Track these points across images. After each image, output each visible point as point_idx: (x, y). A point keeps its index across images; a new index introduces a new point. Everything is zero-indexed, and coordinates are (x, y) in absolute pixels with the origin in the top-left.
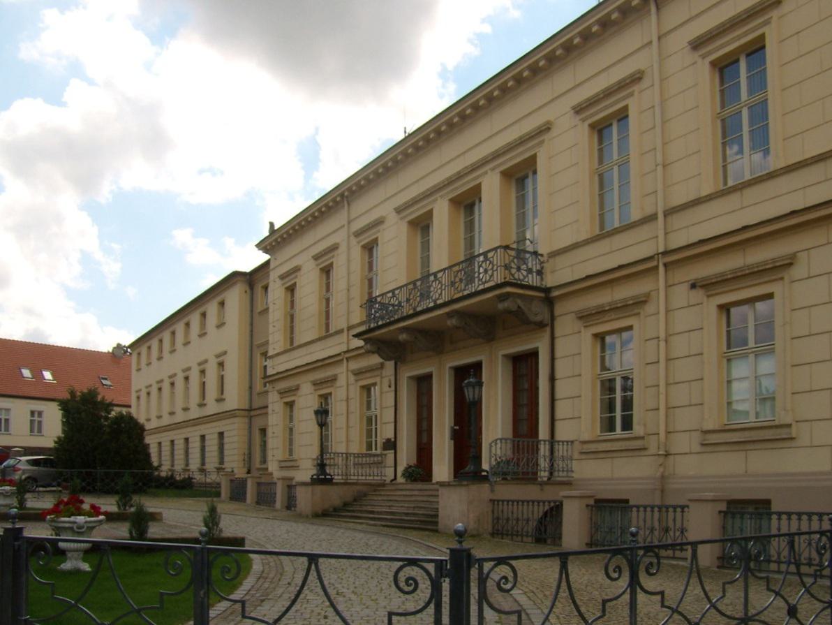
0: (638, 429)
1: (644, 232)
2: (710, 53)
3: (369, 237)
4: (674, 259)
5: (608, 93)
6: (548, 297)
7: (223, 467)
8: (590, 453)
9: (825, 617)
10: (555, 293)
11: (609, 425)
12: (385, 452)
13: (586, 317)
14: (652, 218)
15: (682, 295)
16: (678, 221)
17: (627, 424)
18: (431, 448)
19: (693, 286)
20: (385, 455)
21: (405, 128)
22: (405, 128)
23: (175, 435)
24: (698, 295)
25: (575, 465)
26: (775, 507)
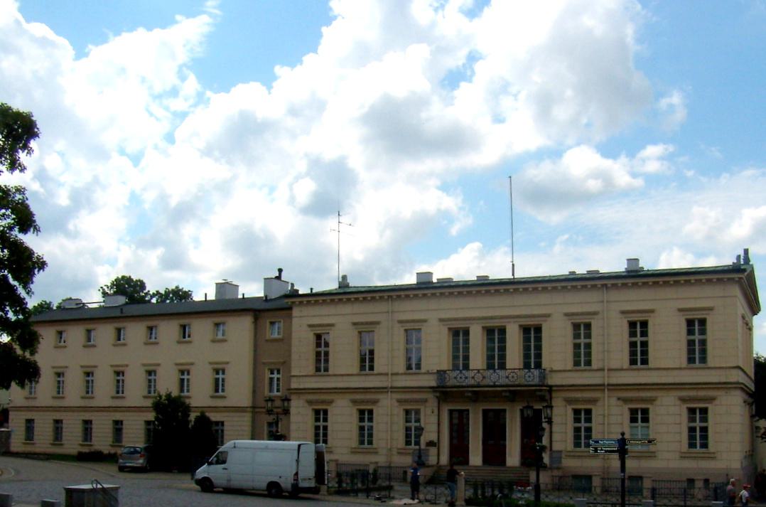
0: (375, 445)
1: (599, 374)
2: (687, 315)
3: (580, 319)
4: (394, 389)
5: (502, 317)
6: (551, 389)
7: (92, 443)
8: (571, 455)
9: (446, 505)
10: (554, 388)
11: (362, 442)
12: (427, 448)
13: (569, 401)
14: (603, 370)
15: (613, 401)
16: (612, 374)
17: (370, 443)
18: (468, 448)
19: (619, 399)
20: (428, 450)
21: (206, 294)
22: (206, 294)
23: (224, 417)
24: (620, 403)
25: (563, 461)
26: (711, 481)
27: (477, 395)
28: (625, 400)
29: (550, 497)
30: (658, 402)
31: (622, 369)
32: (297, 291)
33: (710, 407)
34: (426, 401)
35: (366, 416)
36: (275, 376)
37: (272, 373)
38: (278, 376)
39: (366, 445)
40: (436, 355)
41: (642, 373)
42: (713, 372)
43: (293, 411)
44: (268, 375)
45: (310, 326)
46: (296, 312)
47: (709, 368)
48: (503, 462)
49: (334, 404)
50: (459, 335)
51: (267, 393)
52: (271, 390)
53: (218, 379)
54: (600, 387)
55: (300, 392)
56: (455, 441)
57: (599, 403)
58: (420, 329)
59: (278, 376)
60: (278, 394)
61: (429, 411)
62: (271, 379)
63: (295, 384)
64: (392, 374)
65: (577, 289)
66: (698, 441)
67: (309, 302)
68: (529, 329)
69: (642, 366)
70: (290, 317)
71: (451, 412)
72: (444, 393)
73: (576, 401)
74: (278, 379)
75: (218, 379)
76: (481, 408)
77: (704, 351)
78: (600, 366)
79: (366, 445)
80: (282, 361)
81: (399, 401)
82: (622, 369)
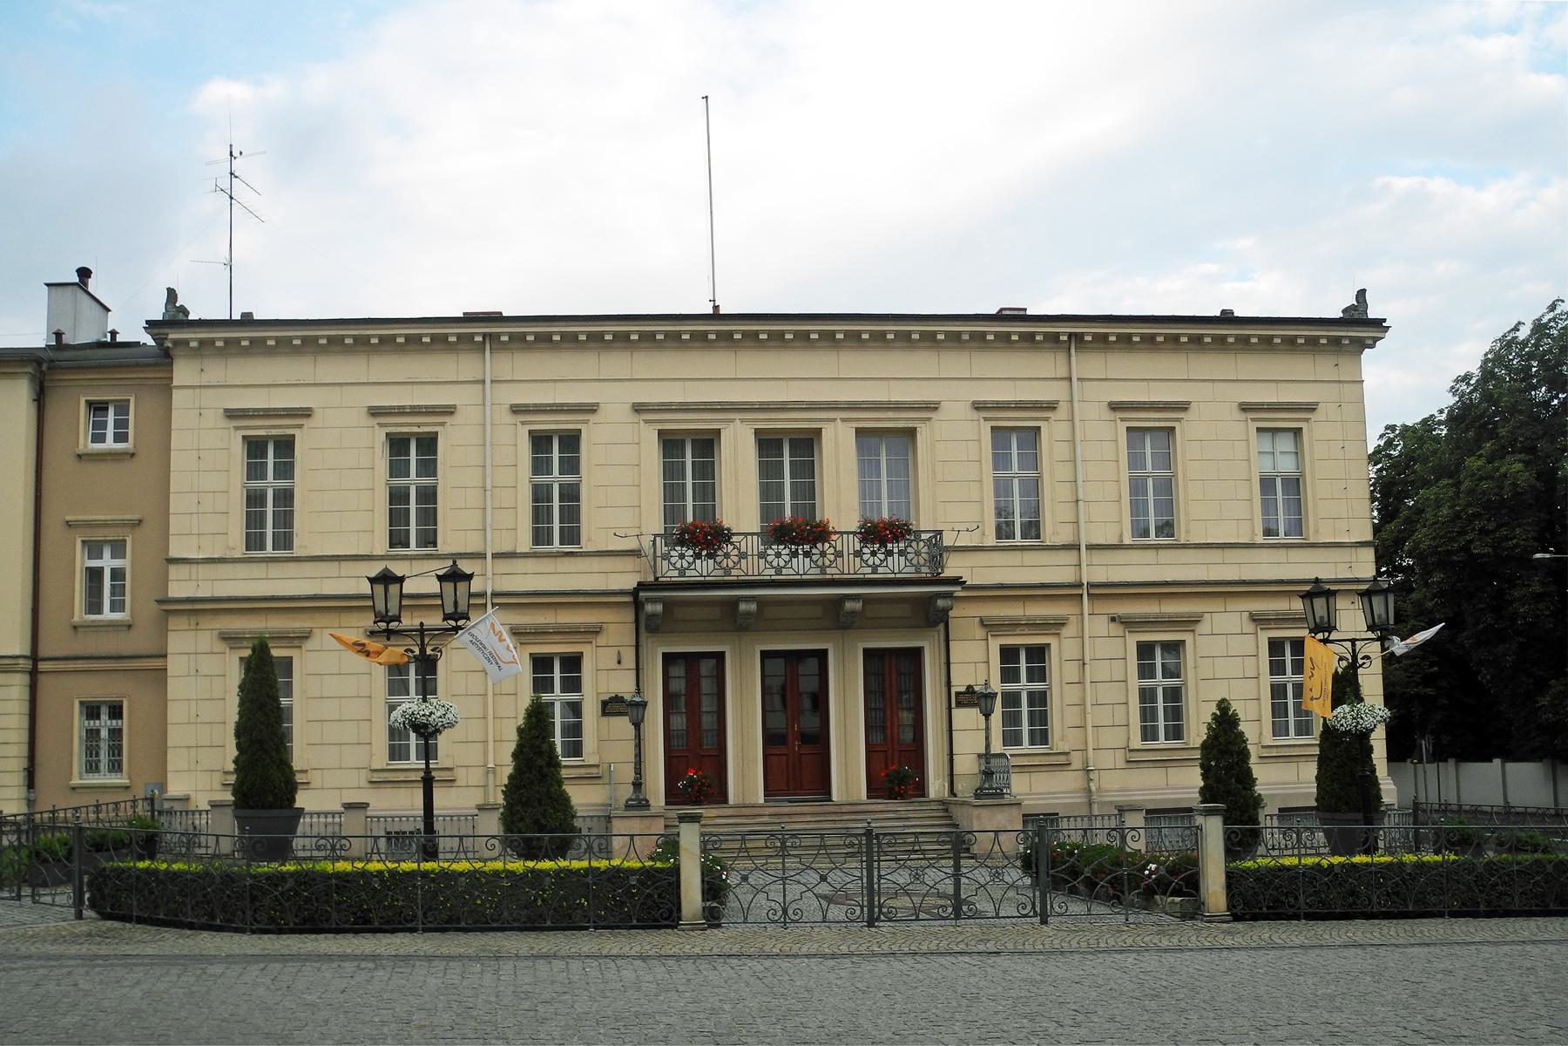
1: (1069, 557)
4: (1105, 592)
19: (1113, 619)
24: (1116, 629)
27: (731, 613)
28: (1129, 623)
29: (831, 877)
30: (1203, 628)
31: (1119, 547)
32: (185, 312)
33: (588, 652)
34: (594, 631)
35: (1288, 658)
36: (107, 562)
37: (94, 549)
38: (118, 563)
39: (1162, 742)
40: (624, 498)
41: (275, 570)
42: (1319, 554)
43: (174, 665)
44: (82, 561)
45: (231, 414)
46: (183, 372)
47: (1185, 546)
48: (822, 787)
49: (309, 645)
50: (689, 450)
51: (80, 615)
52: (94, 606)
53: (100, 571)
54: (1069, 592)
55: (197, 609)
56: (878, 738)
57: (1067, 631)
58: (911, 433)
59: (118, 563)
60: (117, 616)
61: (607, 658)
62: (95, 575)
63: (181, 586)
64: (495, 556)
65: (551, 340)
66: (1025, 727)
67: (1078, 338)
68: (779, 443)
69: (1028, 542)
70: (167, 388)
71: (668, 659)
72: (653, 608)
73: (1013, 625)
74: (117, 574)
75: (100, 571)
76: (758, 648)
77: (571, 514)
78: (1064, 537)
79: (1162, 742)
80: (136, 517)
81: (517, 632)
82: (1119, 547)
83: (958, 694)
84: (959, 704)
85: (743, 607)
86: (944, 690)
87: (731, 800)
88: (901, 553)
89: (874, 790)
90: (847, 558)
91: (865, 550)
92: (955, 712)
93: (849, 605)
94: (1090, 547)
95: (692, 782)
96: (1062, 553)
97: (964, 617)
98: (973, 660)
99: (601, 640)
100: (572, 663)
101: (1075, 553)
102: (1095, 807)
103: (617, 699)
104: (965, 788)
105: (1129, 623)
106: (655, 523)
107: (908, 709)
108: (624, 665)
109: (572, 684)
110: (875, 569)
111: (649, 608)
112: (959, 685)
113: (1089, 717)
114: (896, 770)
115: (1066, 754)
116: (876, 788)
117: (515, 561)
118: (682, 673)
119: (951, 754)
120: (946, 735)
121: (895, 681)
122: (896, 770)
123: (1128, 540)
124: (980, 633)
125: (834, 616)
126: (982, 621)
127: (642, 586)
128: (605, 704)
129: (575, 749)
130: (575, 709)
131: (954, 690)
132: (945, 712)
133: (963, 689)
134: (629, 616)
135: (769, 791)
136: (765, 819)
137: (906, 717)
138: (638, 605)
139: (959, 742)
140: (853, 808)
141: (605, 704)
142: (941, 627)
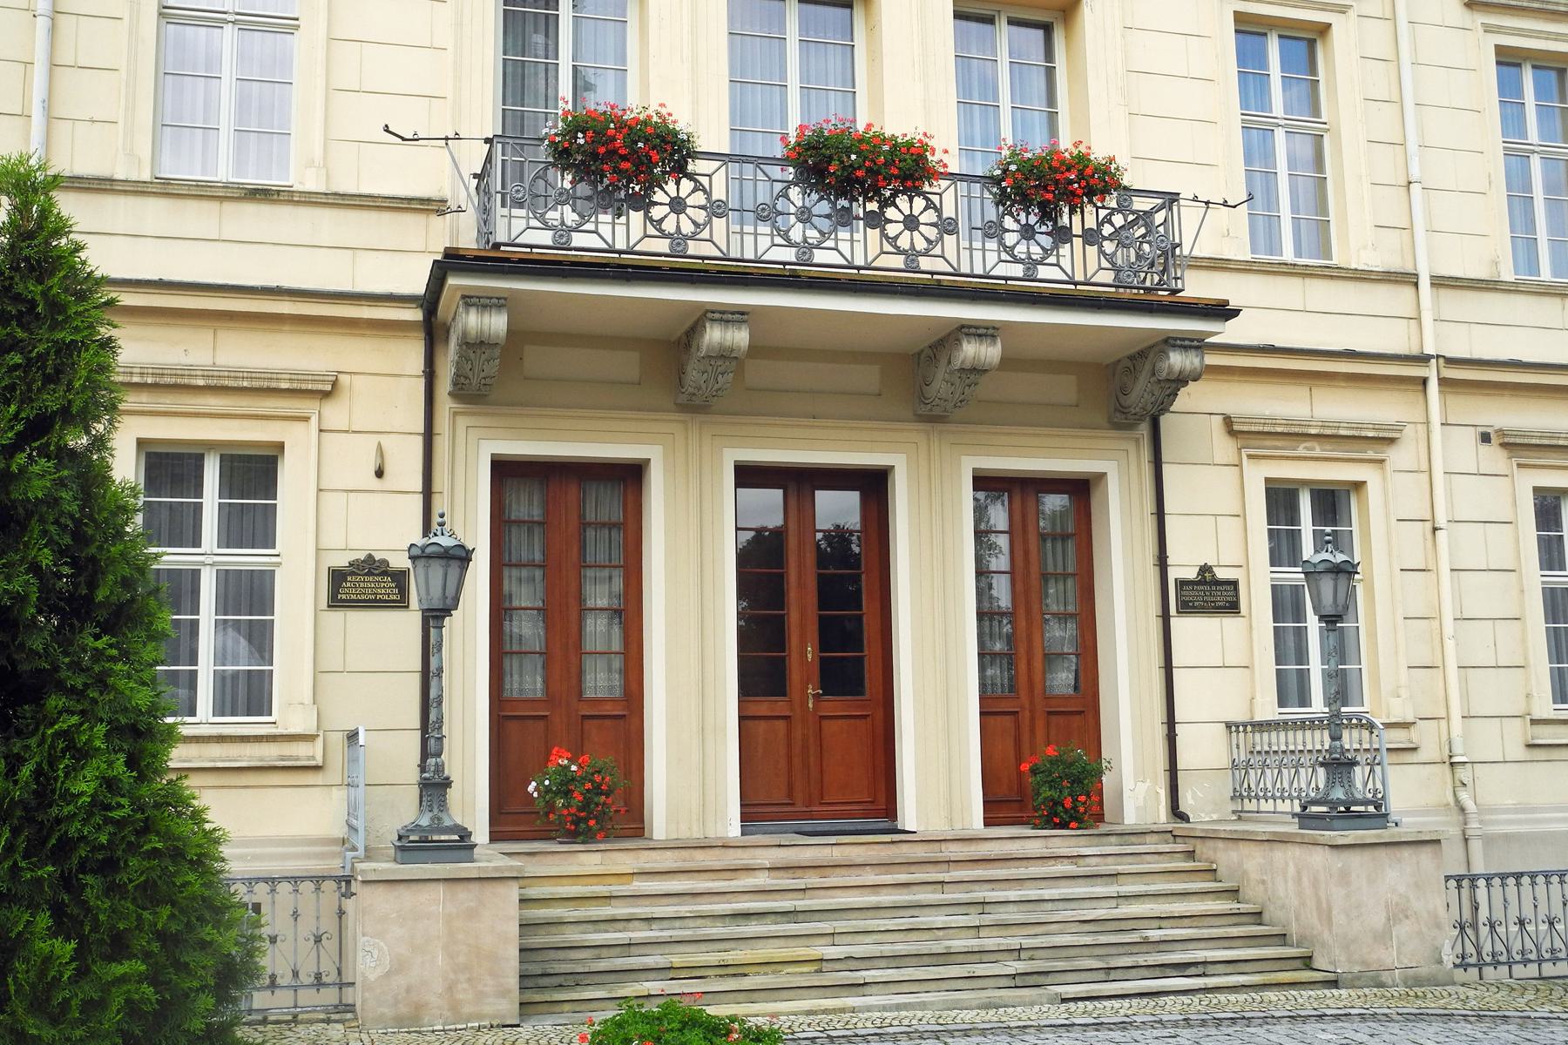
4: (1472, 378)
19: (1486, 438)
24: (1494, 458)
28: (1517, 446)
48: (877, 803)
54: (1400, 373)
71: (503, 469)
73: (1293, 436)
83: (1182, 584)
84: (1186, 608)
85: (714, 335)
86: (1152, 574)
87: (660, 821)
88: (1091, 237)
89: (999, 808)
90: (953, 232)
91: (1009, 222)
92: (1179, 624)
93: (970, 350)
94: (1439, 282)
95: (565, 786)
96: (1383, 290)
97: (1200, 407)
98: (1215, 512)
99: (334, 413)
100: (254, 472)
101: (1408, 291)
102: (1476, 846)
103: (371, 567)
104: (1205, 802)
105: (1517, 446)
106: (482, 113)
107: (1063, 618)
108: (389, 482)
109: (252, 524)
110: (1031, 264)
111: (473, 321)
112: (1183, 567)
113: (1450, 645)
114: (1045, 768)
115: (1405, 725)
116: (1006, 801)
117: (109, 201)
118: (537, 514)
119: (1171, 723)
120: (1158, 677)
121: (1043, 545)
122: (1045, 768)
123: (1508, 275)
124: (1224, 448)
125: (920, 381)
126: (1228, 421)
127: (451, 262)
128: (338, 577)
129: (247, 693)
130: (250, 595)
131: (1173, 574)
132: (1155, 626)
133: (1191, 574)
134: (411, 355)
135: (751, 814)
136: (762, 880)
137: (1060, 635)
138: (433, 331)
139: (1184, 702)
140: (938, 854)
141: (338, 577)
142: (1144, 430)
